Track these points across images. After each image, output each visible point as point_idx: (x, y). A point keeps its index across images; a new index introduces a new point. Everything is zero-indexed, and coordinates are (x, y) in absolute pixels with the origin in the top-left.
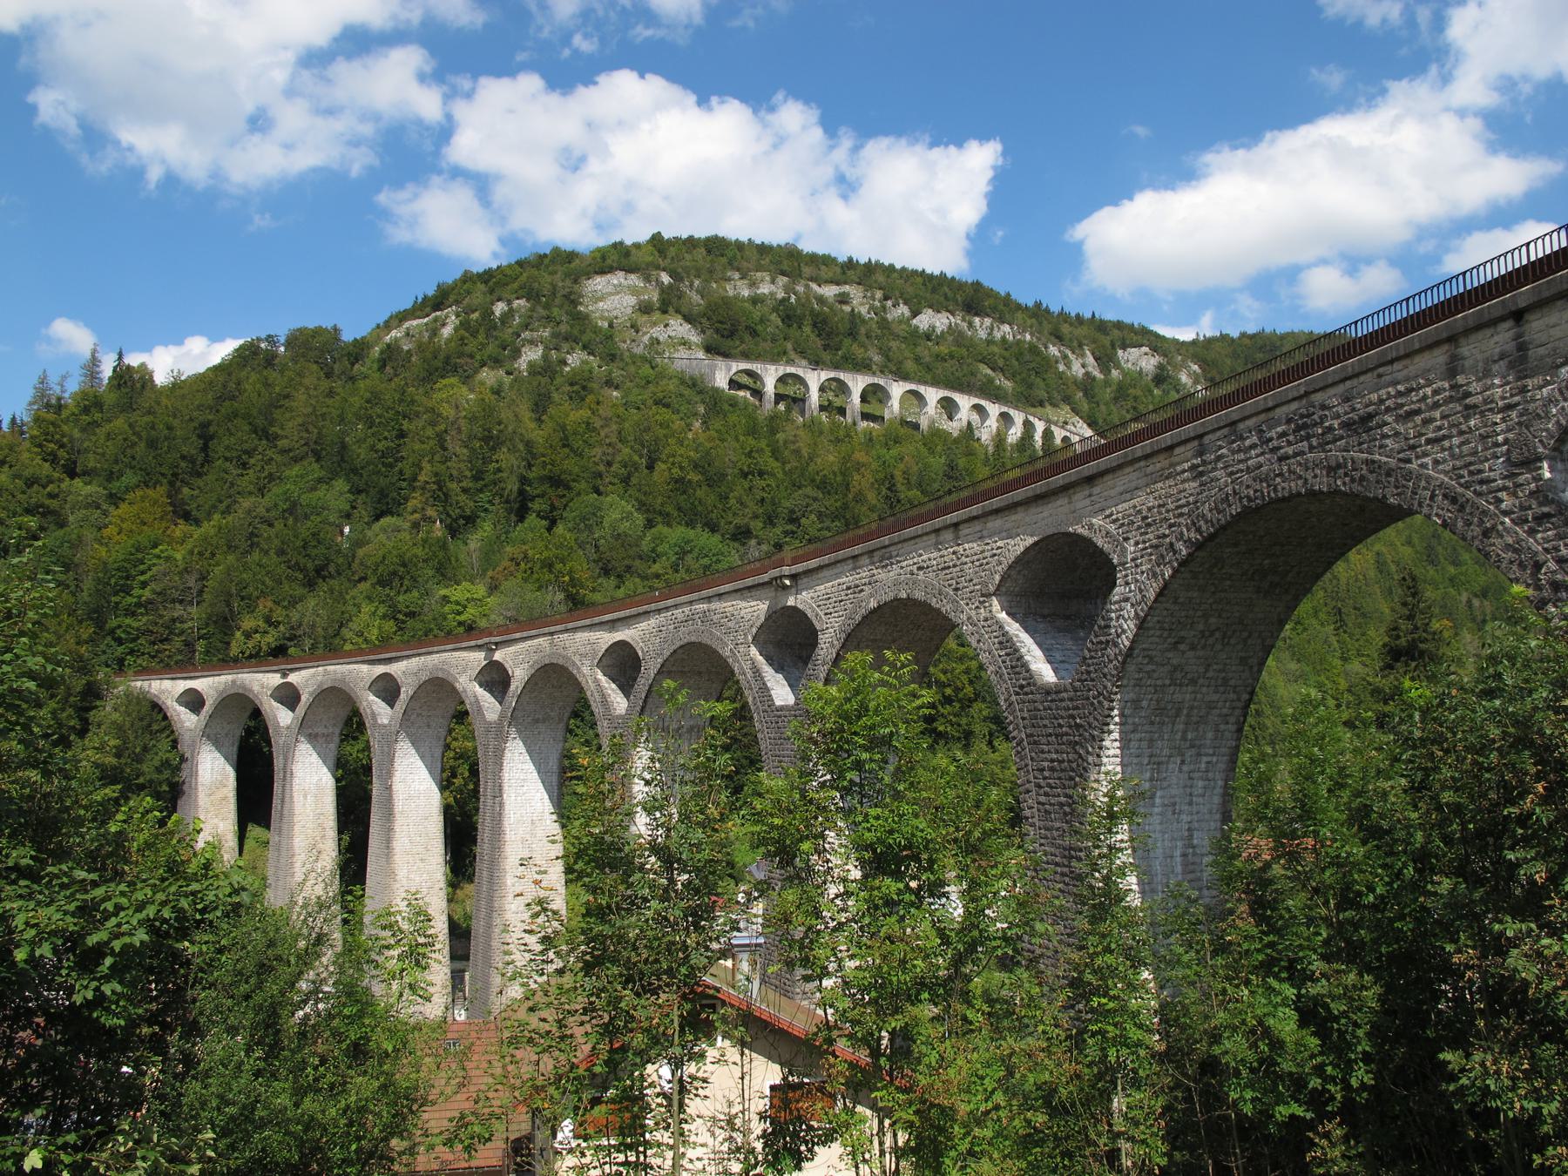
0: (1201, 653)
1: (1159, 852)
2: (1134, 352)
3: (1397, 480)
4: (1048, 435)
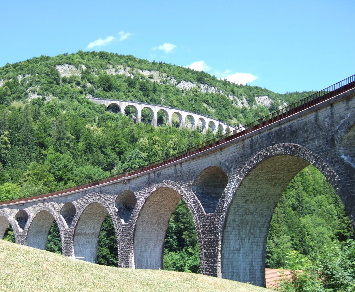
0: (254, 204)
1: (242, 268)
2: (263, 98)
3: (302, 152)
4: (227, 129)
